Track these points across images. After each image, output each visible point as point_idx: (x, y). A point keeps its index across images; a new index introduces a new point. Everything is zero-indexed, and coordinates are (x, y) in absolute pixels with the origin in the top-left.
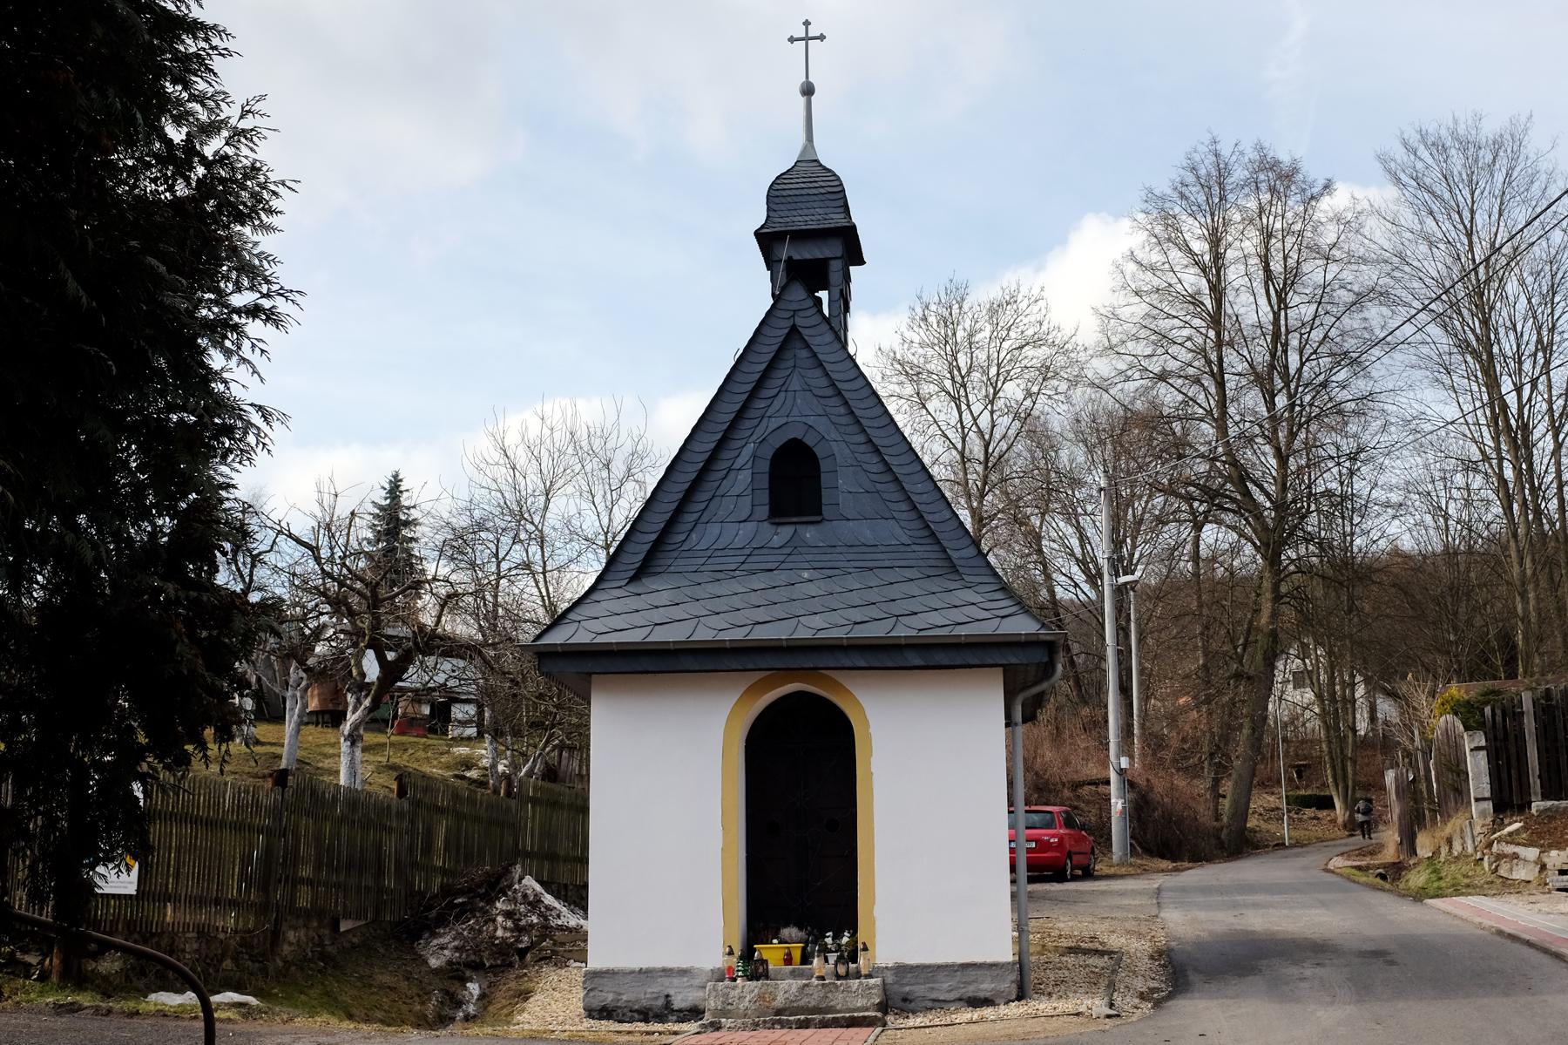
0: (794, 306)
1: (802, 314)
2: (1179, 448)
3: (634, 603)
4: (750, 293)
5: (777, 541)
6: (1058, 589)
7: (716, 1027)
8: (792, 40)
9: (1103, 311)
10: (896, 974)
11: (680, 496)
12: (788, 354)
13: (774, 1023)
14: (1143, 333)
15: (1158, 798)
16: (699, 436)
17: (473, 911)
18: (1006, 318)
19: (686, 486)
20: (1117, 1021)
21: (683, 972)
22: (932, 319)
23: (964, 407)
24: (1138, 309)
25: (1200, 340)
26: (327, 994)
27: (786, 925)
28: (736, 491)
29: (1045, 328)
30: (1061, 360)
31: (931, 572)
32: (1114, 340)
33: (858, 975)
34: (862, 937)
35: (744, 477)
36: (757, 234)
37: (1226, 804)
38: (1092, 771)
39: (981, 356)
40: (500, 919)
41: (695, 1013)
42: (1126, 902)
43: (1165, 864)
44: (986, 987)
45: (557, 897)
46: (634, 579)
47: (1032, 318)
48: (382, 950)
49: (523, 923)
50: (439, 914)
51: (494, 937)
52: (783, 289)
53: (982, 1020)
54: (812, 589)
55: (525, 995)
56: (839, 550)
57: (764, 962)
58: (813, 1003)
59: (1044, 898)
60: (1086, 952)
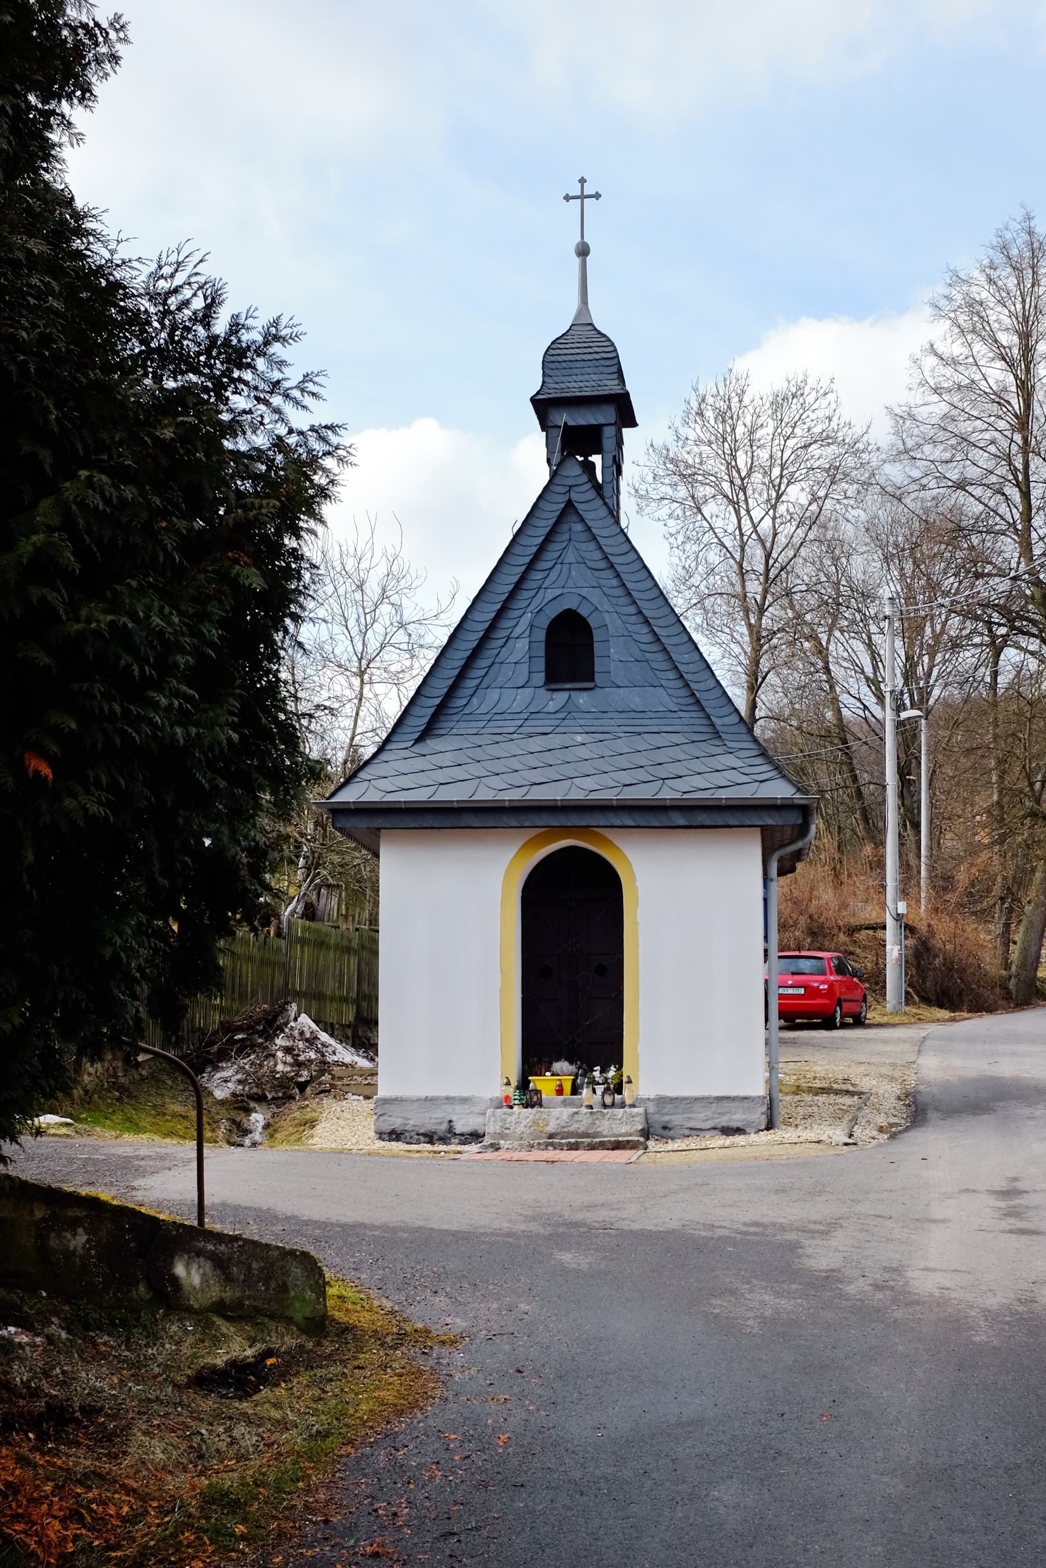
0: (570, 482)
1: (577, 489)
2: (975, 567)
3: (419, 763)
4: (528, 463)
5: (552, 707)
6: (845, 712)
7: (496, 1147)
8: (567, 198)
9: (897, 411)
10: (657, 1105)
11: (462, 662)
12: (564, 527)
13: (547, 1145)
14: (942, 436)
15: (940, 945)
16: (479, 606)
17: (253, 1046)
18: (791, 412)
19: (468, 653)
20: (854, 1148)
21: (465, 1100)
22: (709, 414)
23: (743, 512)
24: (939, 408)
25: (1005, 444)
26: (129, 1120)
27: (558, 1060)
28: (513, 658)
29: (834, 424)
30: (850, 461)
31: (695, 737)
32: (910, 443)
33: (623, 1105)
34: (626, 1071)
35: (522, 645)
36: (533, 400)
37: (1015, 953)
38: (869, 914)
39: (763, 455)
40: (280, 1054)
41: (476, 1136)
42: (888, 1048)
43: (945, 1014)
44: (736, 1119)
45: (332, 1035)
46: (419, 740)
47: (820, 414)
48: (169, 1082)
49: (302, 1058)
50: (220, 1049)
51: (274, 1071)
52: (559, 465)
53: (732, 1146)
54: (584, 752)
55: (312, 1123)
56: (609, 715)
57: (538, 1092)
58: (582, 1129)
59: (807, 1044)
60: (837, 1092)
